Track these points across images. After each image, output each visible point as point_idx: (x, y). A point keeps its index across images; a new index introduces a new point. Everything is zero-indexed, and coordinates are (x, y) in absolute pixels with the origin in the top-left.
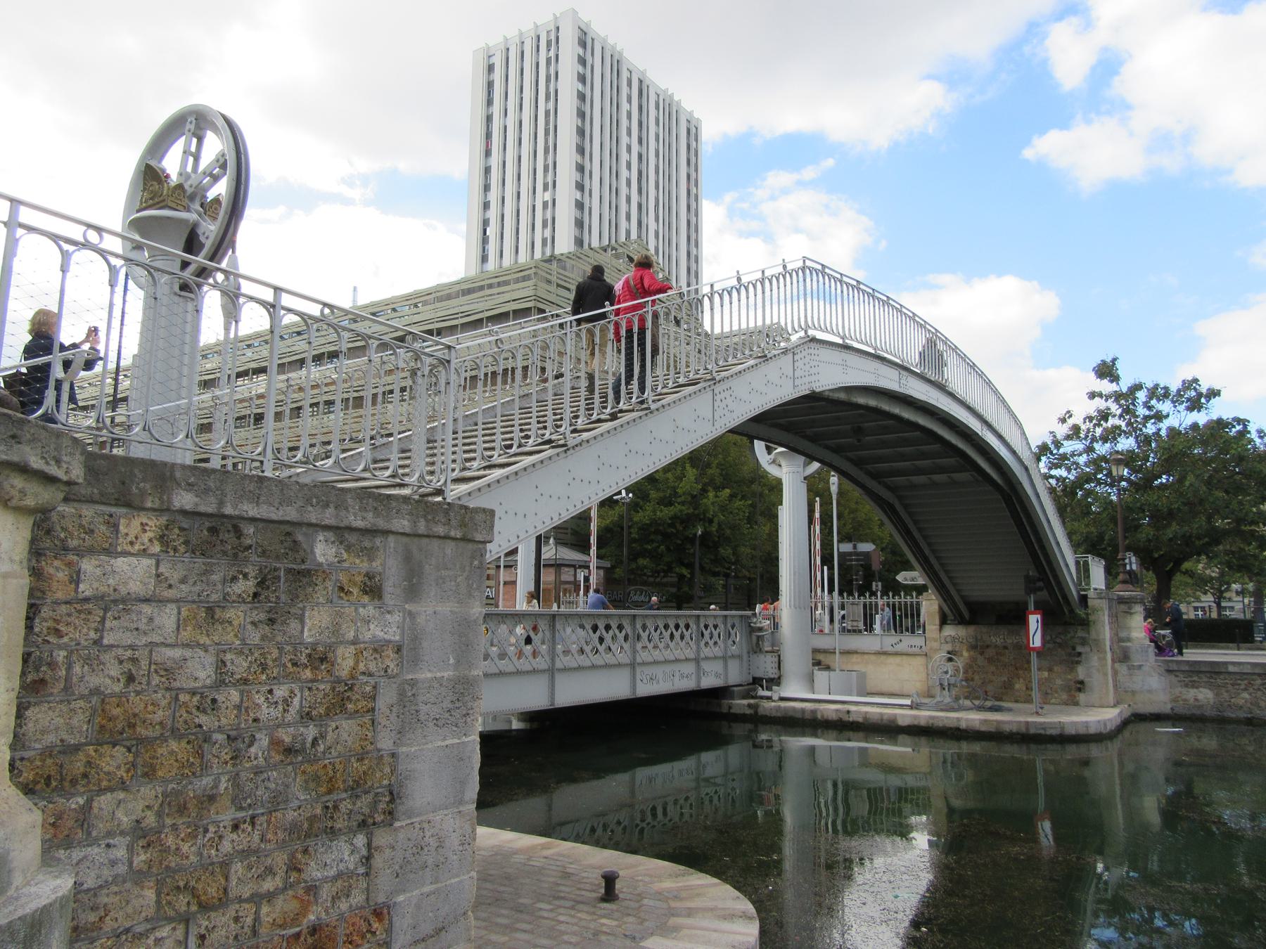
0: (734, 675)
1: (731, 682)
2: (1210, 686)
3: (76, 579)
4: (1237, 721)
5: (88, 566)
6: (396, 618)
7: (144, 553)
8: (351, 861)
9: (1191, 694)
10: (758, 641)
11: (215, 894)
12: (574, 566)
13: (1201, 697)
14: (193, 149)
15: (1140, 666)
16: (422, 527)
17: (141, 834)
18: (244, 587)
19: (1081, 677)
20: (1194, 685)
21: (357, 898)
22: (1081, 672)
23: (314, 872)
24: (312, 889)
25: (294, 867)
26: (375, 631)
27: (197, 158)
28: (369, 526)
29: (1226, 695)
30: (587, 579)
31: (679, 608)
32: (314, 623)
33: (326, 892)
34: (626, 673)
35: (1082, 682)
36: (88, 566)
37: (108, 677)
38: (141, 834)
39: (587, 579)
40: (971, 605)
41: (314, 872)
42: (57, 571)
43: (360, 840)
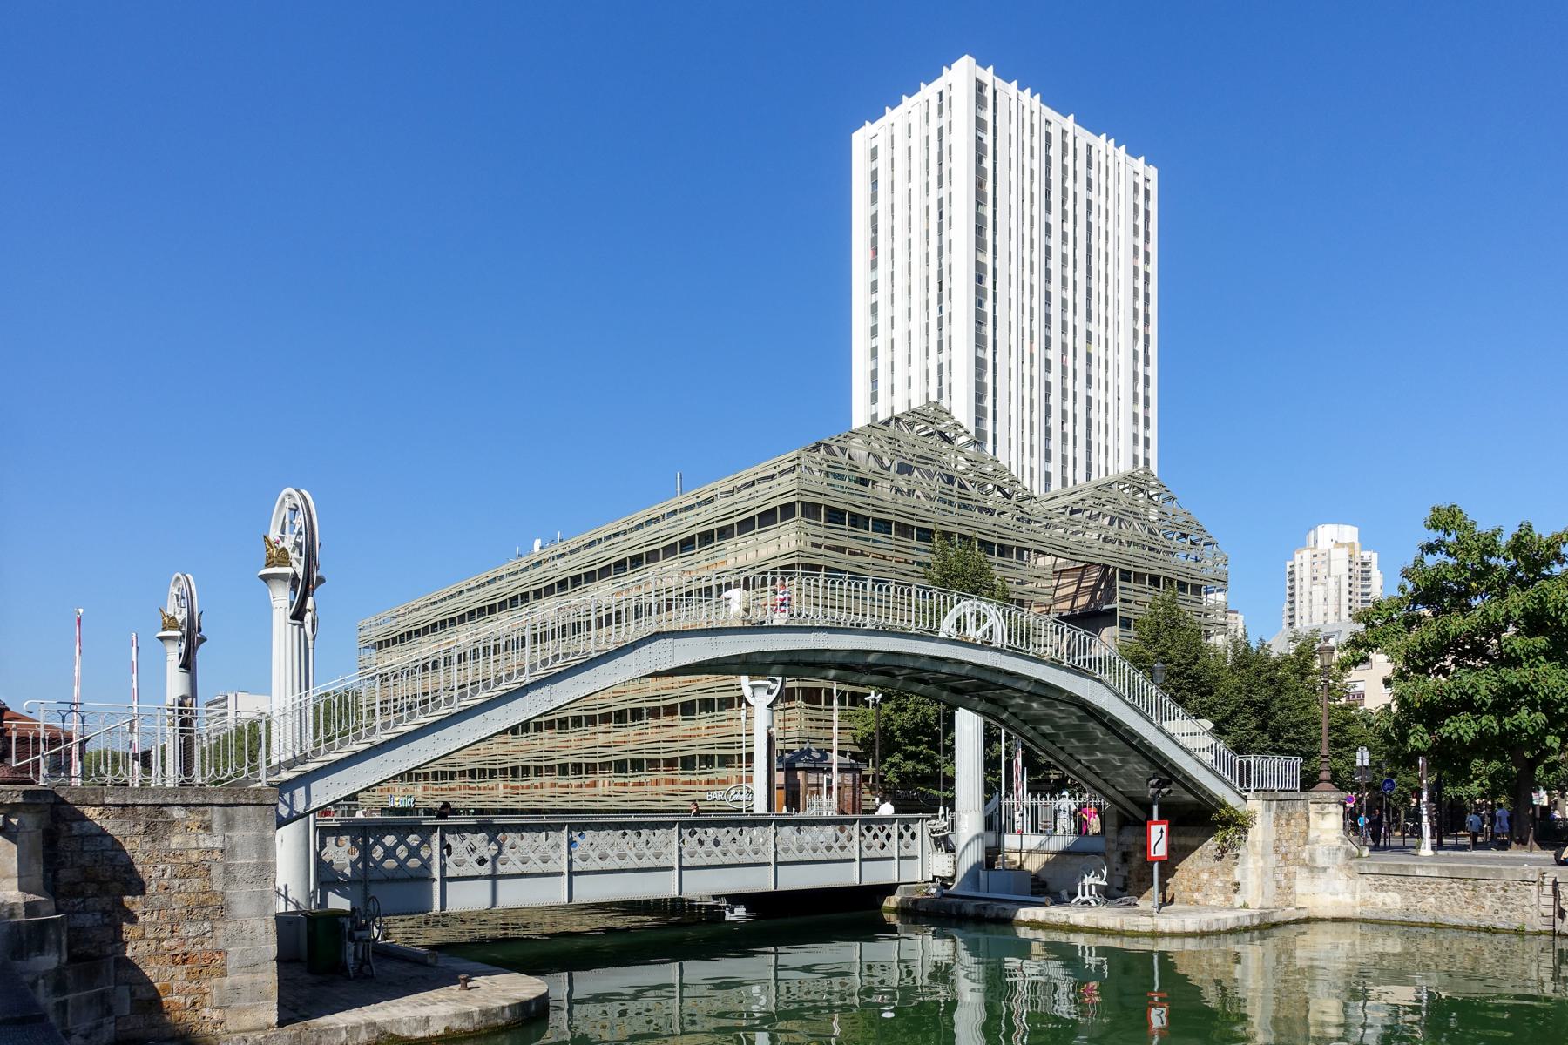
2: (1398, 889)
3: (71, 829)
4: (1423, 925)
5: (75, 825)
6: (220, 838)
9: (1380, 898)
13: (1388, 901)
15: (1325, 869)
16: (231, 801)
17: (104, 912)
18: (140, 829)
19: (1237, 879)
20: (1382, 888)
22: (1237, 875)
26: (208, 844)
28: (1118, 926)
29: (1413, 900)
32: (175, 841)
34: (1025, 848)
35: (1237, 884)
36: (75, 825)
37: (87, 860)
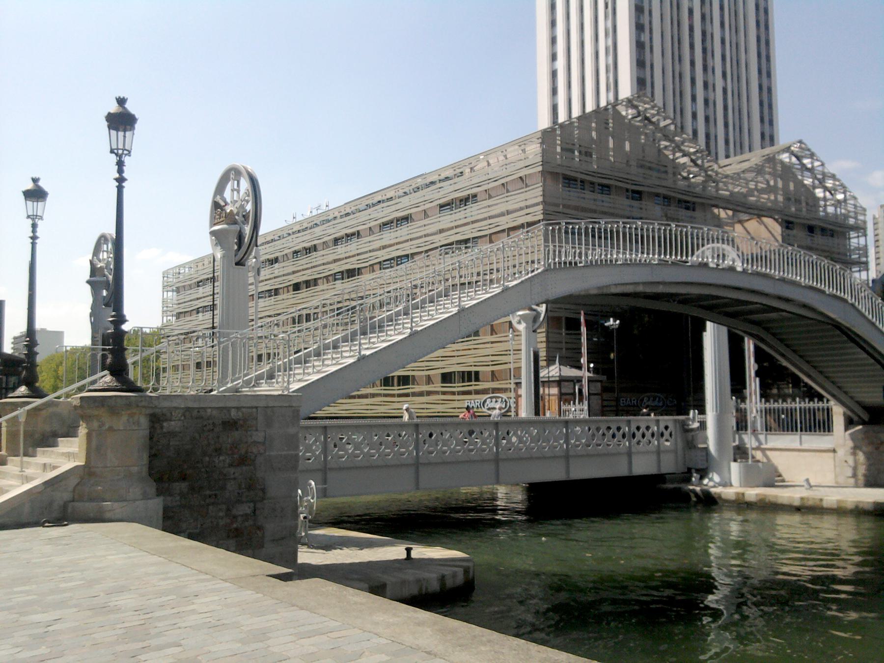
0: (668, 466)
1: (664, 470)
3: (162, 427)
5: (165, 424)
7: (179, 420)
8: (249, 511)
10: (690, 440)
11: (125, 418)
12: (572, 381)
14: (236, 187)
21: (251, 522)
23: (234, 512)
24: (235, 517)
25: (228, 510)
27: (238, 192)
30: (580, 391)
31: (617, 415)
33: (239, 519)
36: (165, 424)
38: (182, 495)
39: (580, 391)
40: (867, 408)
41: (234, 512)
42: (157, 425)
43: (252, 505)
